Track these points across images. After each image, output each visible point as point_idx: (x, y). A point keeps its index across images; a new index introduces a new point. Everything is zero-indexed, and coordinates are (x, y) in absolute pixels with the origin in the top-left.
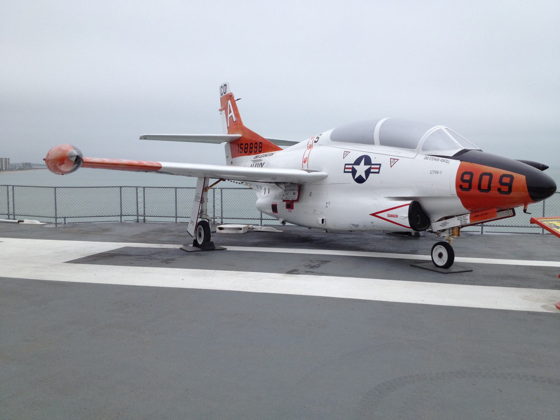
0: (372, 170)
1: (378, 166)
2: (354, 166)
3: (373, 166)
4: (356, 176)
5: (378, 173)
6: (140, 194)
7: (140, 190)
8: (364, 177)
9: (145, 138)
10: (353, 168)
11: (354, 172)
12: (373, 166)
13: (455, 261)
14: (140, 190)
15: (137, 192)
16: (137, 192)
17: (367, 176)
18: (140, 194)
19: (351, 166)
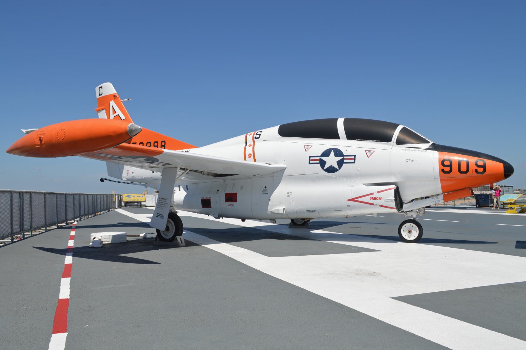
0: (345, 161)
1: (353, 157)
2: (322, 158)
3: (345, 157)
6: (86, 198)
10: (321, 160)
11: (322, 163)
12: (345, 157)
19: (318, 158)
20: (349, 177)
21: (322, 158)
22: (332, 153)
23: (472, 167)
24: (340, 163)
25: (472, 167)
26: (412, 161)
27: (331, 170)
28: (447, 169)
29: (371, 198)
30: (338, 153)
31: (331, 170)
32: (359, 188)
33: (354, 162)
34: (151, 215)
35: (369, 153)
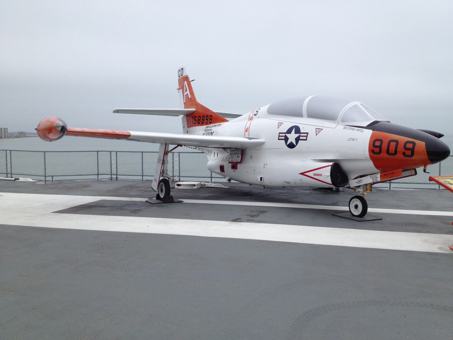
0: (301, 138)
1: (306, 135)
2: (287, 135)
3: (301, 135)
4: (288, 143)
5: (306, 140)
6: (114, 157)
7: (114, 154)
8: (295, 144)
9: (117, 111)
10: (286, 136)
11: (286, 139)
12: (301, 135)
13: (368, 211)
14: (114, 154)
15: (111, 156)
16: (111, 156)
17: (297, 142)
18: (114, 157)
19: (284, 135)
20: (302, 153)
21: (287, 135)
22: (295, 143)
23: (401, 148)
24: (297, 140)
25: (401, 148)
26: (354, 140)
27: (291, 146)
28: (377, 150)
29: (315, 175)
30: (297, 130)
31: (291, 146)
32: (310, 164)
33: (306, 140)
34: (331, 164)
35: (318, 130)
